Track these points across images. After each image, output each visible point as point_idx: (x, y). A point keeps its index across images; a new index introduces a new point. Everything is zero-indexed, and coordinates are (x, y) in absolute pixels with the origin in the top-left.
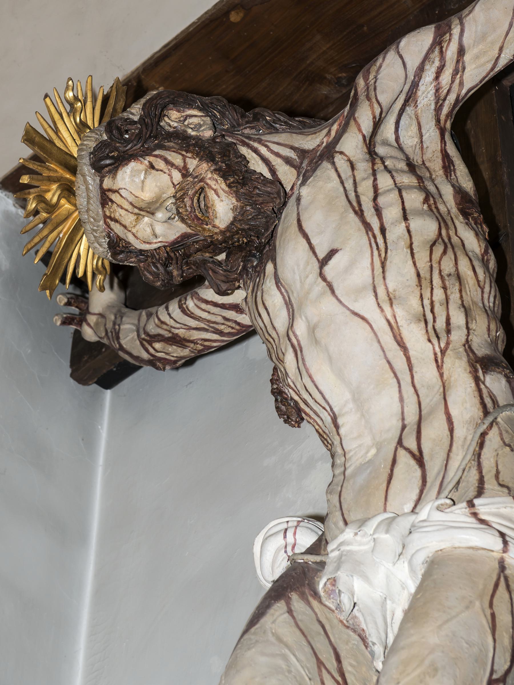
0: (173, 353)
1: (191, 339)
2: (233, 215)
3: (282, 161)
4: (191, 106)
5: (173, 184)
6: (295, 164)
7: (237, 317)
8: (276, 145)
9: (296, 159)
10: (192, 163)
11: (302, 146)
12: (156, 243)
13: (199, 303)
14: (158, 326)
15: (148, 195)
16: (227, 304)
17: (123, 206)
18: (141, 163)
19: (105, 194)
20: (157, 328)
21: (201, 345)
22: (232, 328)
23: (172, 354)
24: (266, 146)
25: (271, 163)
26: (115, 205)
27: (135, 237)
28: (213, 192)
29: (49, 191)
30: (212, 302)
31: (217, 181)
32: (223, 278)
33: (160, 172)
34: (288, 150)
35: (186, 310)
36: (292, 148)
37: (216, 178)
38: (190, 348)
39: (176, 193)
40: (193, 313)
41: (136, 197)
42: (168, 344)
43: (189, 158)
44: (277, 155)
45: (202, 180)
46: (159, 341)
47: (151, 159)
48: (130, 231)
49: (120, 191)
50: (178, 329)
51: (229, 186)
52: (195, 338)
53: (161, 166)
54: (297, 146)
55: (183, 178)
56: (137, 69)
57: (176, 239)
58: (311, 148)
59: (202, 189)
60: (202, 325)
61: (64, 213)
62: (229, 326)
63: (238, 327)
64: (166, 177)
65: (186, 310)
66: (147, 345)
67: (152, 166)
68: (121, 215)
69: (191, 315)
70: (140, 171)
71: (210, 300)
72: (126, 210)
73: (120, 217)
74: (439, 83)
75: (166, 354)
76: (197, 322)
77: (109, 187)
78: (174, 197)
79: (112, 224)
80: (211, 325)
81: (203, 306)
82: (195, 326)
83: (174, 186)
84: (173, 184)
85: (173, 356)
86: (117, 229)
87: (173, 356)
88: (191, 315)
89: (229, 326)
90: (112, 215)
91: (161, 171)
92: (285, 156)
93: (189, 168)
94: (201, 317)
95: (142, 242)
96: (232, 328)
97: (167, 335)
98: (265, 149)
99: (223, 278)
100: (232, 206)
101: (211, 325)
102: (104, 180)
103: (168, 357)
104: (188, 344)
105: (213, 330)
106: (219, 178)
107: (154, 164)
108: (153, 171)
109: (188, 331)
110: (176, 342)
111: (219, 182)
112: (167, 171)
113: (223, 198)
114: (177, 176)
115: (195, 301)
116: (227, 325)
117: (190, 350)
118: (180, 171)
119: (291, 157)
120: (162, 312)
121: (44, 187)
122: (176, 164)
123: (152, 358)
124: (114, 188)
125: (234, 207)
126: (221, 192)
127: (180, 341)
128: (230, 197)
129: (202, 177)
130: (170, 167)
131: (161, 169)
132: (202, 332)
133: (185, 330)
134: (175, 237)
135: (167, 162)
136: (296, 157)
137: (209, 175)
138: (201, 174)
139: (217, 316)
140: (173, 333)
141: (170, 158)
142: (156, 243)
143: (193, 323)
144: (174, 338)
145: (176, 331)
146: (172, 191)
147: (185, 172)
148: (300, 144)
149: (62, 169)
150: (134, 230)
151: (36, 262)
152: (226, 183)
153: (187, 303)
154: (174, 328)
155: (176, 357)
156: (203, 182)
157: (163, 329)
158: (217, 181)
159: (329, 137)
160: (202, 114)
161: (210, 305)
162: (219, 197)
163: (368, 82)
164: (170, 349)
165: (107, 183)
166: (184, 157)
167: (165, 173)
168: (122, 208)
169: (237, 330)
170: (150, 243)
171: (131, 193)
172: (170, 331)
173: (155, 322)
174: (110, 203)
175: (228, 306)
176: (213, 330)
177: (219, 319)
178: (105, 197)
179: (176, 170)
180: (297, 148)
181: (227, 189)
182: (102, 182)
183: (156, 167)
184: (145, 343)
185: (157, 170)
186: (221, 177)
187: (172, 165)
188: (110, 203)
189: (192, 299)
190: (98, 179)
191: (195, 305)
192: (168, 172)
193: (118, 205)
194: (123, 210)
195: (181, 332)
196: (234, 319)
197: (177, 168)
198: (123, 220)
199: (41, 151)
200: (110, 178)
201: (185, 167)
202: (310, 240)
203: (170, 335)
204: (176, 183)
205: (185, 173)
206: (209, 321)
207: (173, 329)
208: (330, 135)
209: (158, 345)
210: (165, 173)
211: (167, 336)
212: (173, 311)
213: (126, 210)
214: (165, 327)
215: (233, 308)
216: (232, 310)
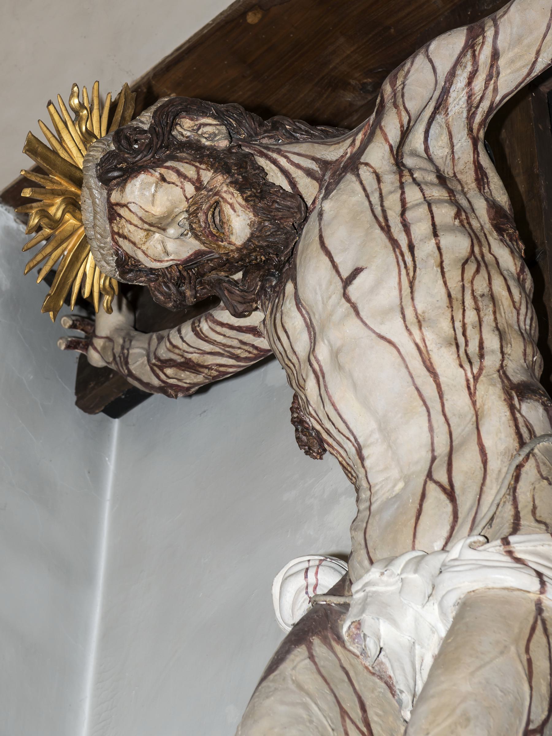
0: (186, 379)
1: (206, 364)
2: (250, 231)
3: (302, 173)
4: (205, 114)
5: (186, 198)
6: (317, 176)
7: (255, 341)
8: (296, 156)
9: (317, 171)
10: (207, 176)
11: (325, 157)
12: (167, 261)
13: (213, 326)
14: (169, 350)
15: (158, 210)
16: (244, 327)
17: (132, 221)
18: (152, 175)
19: (113, 209)
20: (168, 352)
21: (216, 370)
22: (250, 352)
23: (184, 381)
24: (286, 157)
25: (291, 175)
26: (123, 221)
27: (145, 254)
28: (229, 206)
29: (52, 205)
30: (227, 324)
31: (233, 194)
32: (240, 299)
33: (172, 185)
34: (310, 161)
35: (200, 333)
36: (314, 159)
37: (232, 191)
38: (204, 374)
39: (189, 207)
40: (207, 337)
41: (147, 212)
42: (180, 370)
43: (203, 169)
44: (298, 166)
45: (217, 193)
46: (171, 367)
47: (163, 171)
48: (140, 248)
49: (129, 205)
50: (192, 353)
51: (246, 200)
52: (209, 363)
53: (172, 179)
54: (319, 157)
55: (196, 191)
56: (147, 74)
57: (189, 257)
58: (334, 159)
59: (217, 203)
60: (217, 350)
61: (69, 228)
62: (246, 351)
63: (255, 352)
64: (178, 190)
65: (200, 333)
66: (158, 371)
67: (163, 179)
68: (130, 231)
69: (205, 339)
70: (150, 184)
71: (225, 322)
72: (136, 226)
73: (129, 234)
74: (471, 90)
75: (179, 380)
76: (212, 346)
77: (117, 201)
78: (187, 211)
79: (121, 241)
80: (227, 349)
81: (219, 329)
82: (209, 351)
83: (187, 199)
84: (186, 198)
85: (186, 383)
86: (126, 246)
87: (186, 383)
88: (205, 339)
89: (246, 351)
90: (121, 232)
91: (173, 183)
92: (306, 168)
93: (203, 181)
94: (215, 341)
95: (153, 260)
96: (250, 352)
97: (180, 359)
98: (285, 160)
99: (240, 299)
100: (249, 222)
101: (227, 349)
102: (111, 194)
103: (180, 384)
104: (202, 370)
105: (228, 354)
106: (235, 191)
107: (165, 176)
108: (165, 184)
109: (202, 355)
110: (189, 368)
111: (236, 195)
112: (179, 184)
113: (240, 213)
114: (190, 189)
115: (210, 323)
116: (244, 349)
117: (204, 376)
118: (193, 183)
119: (312, 169)
120: (174, 335)
121: (47, 201)
122: (190, 176)
123: (163, 385)
124: (123, 202)
125: (251, 222)
126: (237, 206)
127: (193, 366)
128: (247, 212)
129: (217, 190)
130: (182, 180)
131: (173, 181)
132: (217, 357)
133: (198, 355)
134: (188, 255)
135: (179, 174)
136: (318, 169)
137: (225, 188)
138: (216, 187)
139: (233, 340)
140: (186, 358)
141: (182, 170)
142: (167, 261)
143: (207, 347)
144: (187, 364)
145: (189, 356)
146: (184, 205)
147: (198, 185)
148: (323, 155)
149: (66, 182)
150: (144, 248)
151: (38, 282)
152: (243, 197)
153: (201, 325)
154: (187, 352)
155: (189, 383)
156: (218, 195)
157: (175, 353)
158: (233, 194)
159: (354, 148)
160: (217, 123)
161: (226, 327)
162: (235, 211)
163: (395, 88)
164: (183, 375)
165: (115, 197)
166: (198, 169)
167: (177, 186)
168: (131, 223)
169: (254, 354)
170: (161, 261)
171: (141, 207)
172: (182, 356)
173: (166, 346)
174: (118, 218)
175: (245, 329)
176: (228, 354)
177: (235, 343)
178: (113, 212)
179: (189, 183)
180: (319, 159)
181: (243, 203)
182: (109, 195)
183: (168, 179)
184: (155, 368)
185: (169, 183)
186: (237, 190)
187: (185, 177)
188: (118, 218)
189: (206, 321)
190: (105, 192)
191: (210, 327)
192: (180, 184)
193: (127, 221)
194: (132, 226)
195: (195, 357)
196: (252, 343)
197: (190, 180)
198: (132, 237)
199: (44, 162)
200: (119, 191)
201: (199, 180)
202: (332, 258)
203: (183, 360)
204: (189, 197)
205: (199, 185)
206: (224, 345)
207: (186, 354)
208: (355, 145)
209: (169, 371)
210: (177, 186)
211: (179, 361)
212: (186, 335)
213: (136, 226)
214: (177, 351)
215: (250, 331)
216: (250, 333)
